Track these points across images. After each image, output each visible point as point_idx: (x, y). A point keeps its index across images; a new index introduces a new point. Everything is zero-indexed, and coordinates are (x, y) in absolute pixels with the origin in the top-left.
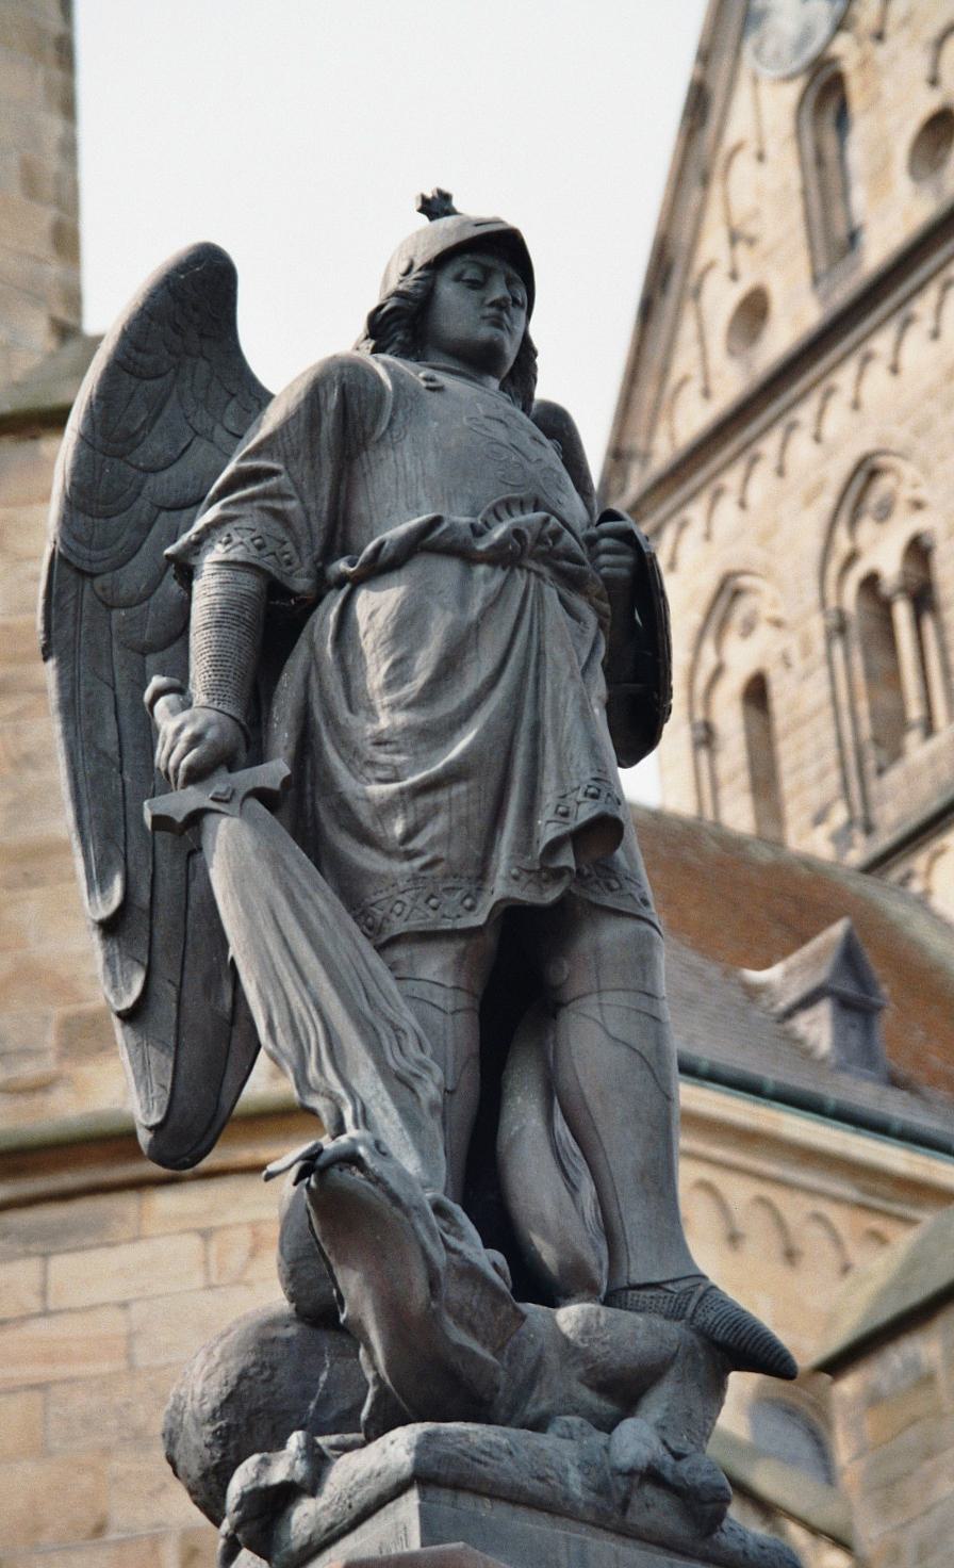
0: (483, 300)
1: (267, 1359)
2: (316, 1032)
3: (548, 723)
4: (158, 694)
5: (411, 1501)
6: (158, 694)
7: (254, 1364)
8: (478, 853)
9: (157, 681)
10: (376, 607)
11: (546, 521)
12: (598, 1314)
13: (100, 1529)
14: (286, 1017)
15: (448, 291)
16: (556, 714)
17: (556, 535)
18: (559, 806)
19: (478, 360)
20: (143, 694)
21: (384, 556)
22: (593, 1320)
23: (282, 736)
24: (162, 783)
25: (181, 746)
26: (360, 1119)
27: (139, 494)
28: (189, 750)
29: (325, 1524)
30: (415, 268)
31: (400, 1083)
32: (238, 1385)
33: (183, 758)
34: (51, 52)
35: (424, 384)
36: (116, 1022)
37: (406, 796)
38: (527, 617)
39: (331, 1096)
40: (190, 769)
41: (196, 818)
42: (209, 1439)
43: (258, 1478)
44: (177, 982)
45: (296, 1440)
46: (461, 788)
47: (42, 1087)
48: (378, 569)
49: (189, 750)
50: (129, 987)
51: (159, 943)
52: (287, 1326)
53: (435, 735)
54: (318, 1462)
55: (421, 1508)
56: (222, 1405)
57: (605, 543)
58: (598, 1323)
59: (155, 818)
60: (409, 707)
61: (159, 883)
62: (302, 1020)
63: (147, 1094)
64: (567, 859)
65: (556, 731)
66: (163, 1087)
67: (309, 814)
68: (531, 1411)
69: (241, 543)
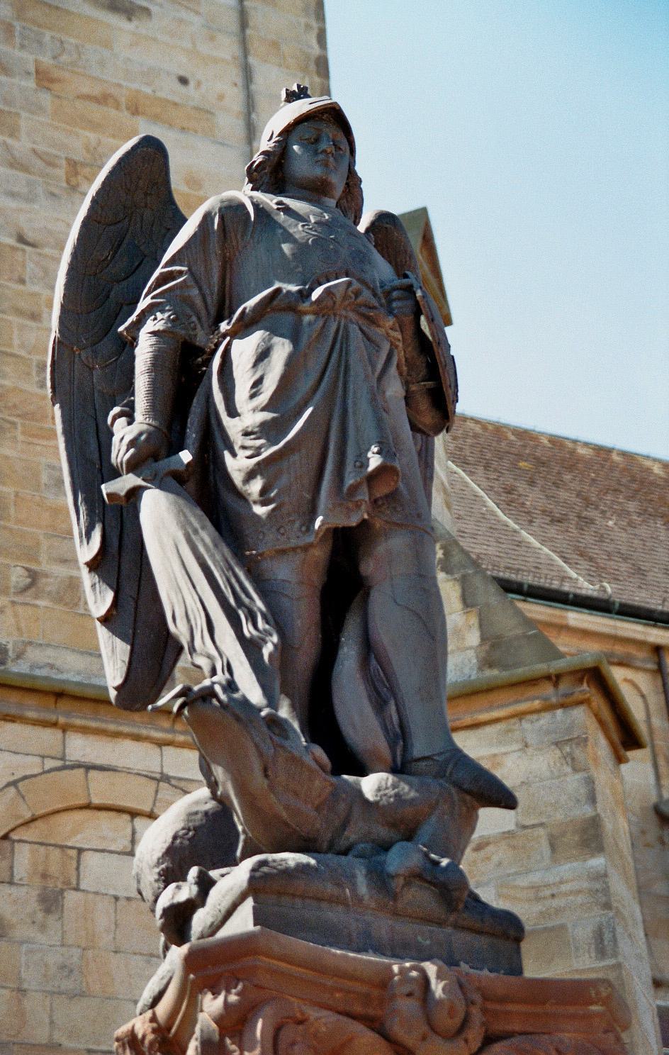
0: (317, 150)
1: (190, 824)
2: (201, 618)
3: (350, 410)
4: (114, 419)
5: (249, 903)
6: (114, 419)
7: (183, 829)
8: (308, 496)
9: (116, 410)
10: (244, 350)
11: (349, 284)
12: (388, 779)
14: (183, 609)
16: (355, 404)
17: (357, 294)
18: (355, 462)
19: (315, 191)
20: (107, 420)
21: (246, 319)
22: (383, 783)
23: (192, 435)
24: (115, 474)
25: (124, 448)
26: (225, 669)
27: (108, 297)
28: (127, 450)
29: (209, 923)
30: (274, 136)
31: (251, 647)
32: (173, 843)
33: (125, 454)
34: (312, 67)
35: (275, 207)
36: (98, 624)
37: (262, 467)
38: (338, 346)
39: (209, 657)
40: (129, 461)
41: (135, 493)
42: (157, 877)
43: (173, 898)
44: (135, 596)
45: (193, 872)
48: (244, 327)
49: (127, 450)
50: (104, 600)
51: (125, 572)
52: (206, 803)
54: (205, 884)
55: (254, 908)
56: (163, 856)
57: (395, 294)
58: (386, 784)
59: (108, 495)
60: (263, 409)
61: (125, 536)
62: (193, 611)
63: (114, 667)
65: (355, 414)
66: (124, 661)
67: (212, 485)
68: (343, 843)
69: (162, 319)
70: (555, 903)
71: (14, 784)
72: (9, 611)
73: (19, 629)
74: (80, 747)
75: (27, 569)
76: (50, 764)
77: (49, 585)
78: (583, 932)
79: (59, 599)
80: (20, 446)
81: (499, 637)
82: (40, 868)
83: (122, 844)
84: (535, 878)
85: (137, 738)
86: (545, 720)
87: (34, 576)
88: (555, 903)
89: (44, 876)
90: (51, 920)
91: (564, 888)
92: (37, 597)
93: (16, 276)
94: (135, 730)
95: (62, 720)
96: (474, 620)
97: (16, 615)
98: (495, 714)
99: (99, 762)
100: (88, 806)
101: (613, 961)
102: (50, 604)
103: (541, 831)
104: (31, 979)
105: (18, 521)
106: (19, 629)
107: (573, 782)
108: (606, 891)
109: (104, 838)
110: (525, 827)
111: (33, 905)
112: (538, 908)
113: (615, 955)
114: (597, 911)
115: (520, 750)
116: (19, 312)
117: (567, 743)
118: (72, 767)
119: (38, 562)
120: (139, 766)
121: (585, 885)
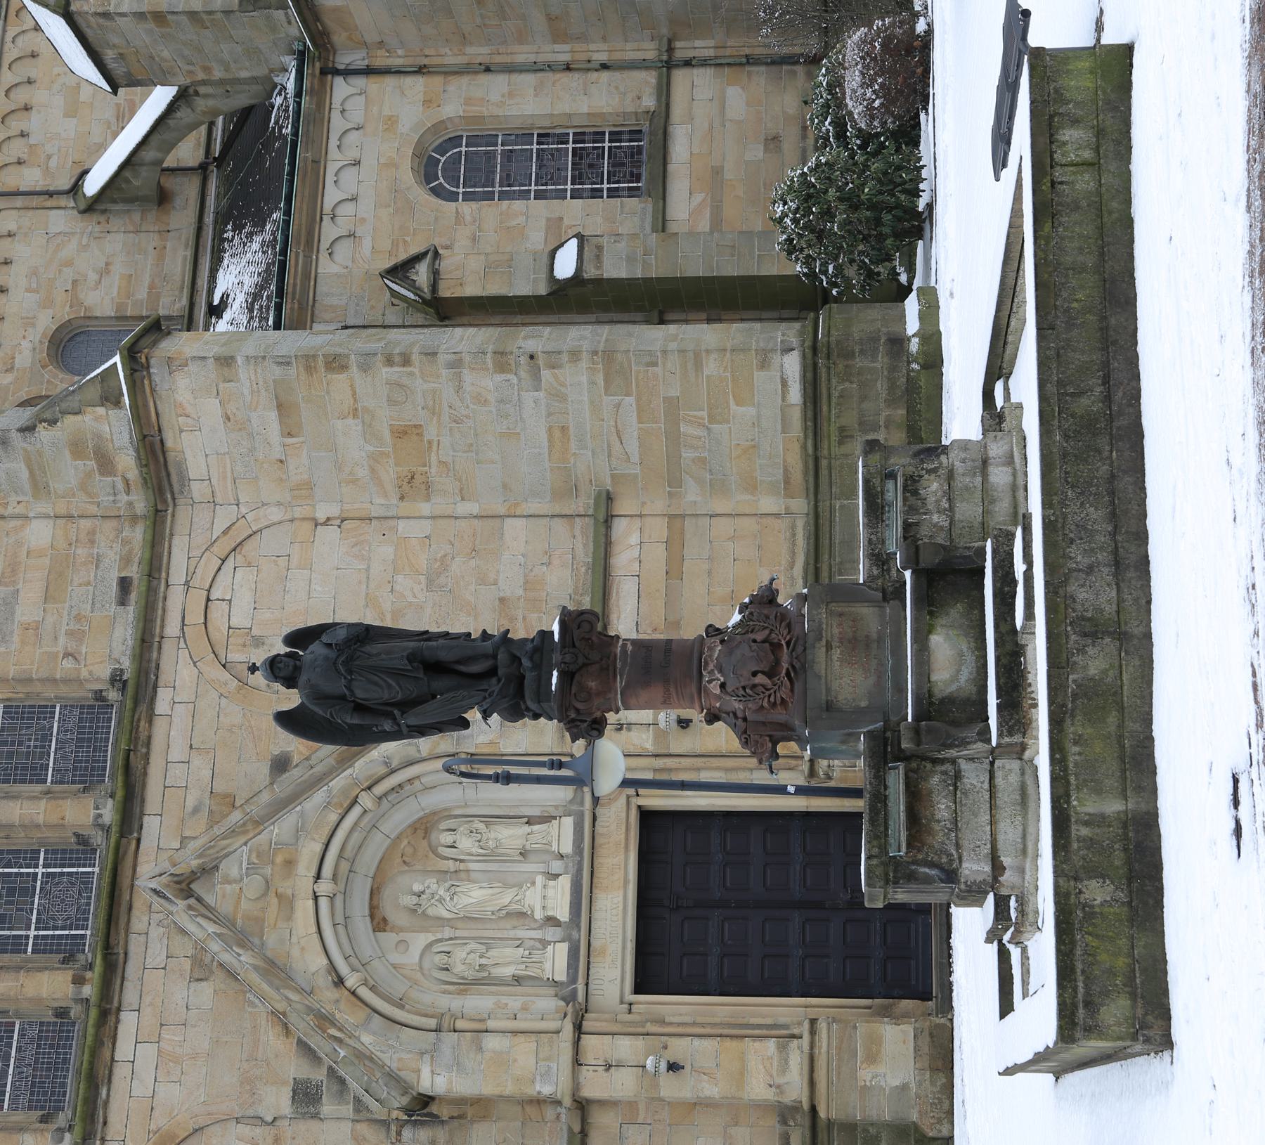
13: (281, 461)
15: (281, 675)
47: (127, 482)
53: (389, 686)
70: (261, 383)
71: (195, 663)
72: (91, 668)
73: (101, 663)
74: (172, 628)
75: (63, 658)
76: (182, 645)
78: (278, 371)
79: (81, 640)
81: (101, 398)
82: (240, 648)
84: (246, 392)
85: (165, 598)
86: (156, 379)
87: (67, 655)
88: (261, 383)
89: (244, 646)
90: (267, 641)
91: (253, 378)
92: (80, 653)
94: (161, 599)
95: (157, 639)
96: (90, 409)
97: (92, 664)
98: (151, 404)
99: (180, 619)
100: (205, 624)
101: (293, 358)
102: (84, 646)
103: (221, 386)
105: (32, 664)
106: (101, 663)
107: (193, 367)
108: (256, 357)
109: (222, 615)
110: (218, 394)
112: (263, 392)
113: (291, 357)
114: (266, 363)
118: (184, 633)
119: (58, 652)
120: (181, 598)
121: (252, 367)
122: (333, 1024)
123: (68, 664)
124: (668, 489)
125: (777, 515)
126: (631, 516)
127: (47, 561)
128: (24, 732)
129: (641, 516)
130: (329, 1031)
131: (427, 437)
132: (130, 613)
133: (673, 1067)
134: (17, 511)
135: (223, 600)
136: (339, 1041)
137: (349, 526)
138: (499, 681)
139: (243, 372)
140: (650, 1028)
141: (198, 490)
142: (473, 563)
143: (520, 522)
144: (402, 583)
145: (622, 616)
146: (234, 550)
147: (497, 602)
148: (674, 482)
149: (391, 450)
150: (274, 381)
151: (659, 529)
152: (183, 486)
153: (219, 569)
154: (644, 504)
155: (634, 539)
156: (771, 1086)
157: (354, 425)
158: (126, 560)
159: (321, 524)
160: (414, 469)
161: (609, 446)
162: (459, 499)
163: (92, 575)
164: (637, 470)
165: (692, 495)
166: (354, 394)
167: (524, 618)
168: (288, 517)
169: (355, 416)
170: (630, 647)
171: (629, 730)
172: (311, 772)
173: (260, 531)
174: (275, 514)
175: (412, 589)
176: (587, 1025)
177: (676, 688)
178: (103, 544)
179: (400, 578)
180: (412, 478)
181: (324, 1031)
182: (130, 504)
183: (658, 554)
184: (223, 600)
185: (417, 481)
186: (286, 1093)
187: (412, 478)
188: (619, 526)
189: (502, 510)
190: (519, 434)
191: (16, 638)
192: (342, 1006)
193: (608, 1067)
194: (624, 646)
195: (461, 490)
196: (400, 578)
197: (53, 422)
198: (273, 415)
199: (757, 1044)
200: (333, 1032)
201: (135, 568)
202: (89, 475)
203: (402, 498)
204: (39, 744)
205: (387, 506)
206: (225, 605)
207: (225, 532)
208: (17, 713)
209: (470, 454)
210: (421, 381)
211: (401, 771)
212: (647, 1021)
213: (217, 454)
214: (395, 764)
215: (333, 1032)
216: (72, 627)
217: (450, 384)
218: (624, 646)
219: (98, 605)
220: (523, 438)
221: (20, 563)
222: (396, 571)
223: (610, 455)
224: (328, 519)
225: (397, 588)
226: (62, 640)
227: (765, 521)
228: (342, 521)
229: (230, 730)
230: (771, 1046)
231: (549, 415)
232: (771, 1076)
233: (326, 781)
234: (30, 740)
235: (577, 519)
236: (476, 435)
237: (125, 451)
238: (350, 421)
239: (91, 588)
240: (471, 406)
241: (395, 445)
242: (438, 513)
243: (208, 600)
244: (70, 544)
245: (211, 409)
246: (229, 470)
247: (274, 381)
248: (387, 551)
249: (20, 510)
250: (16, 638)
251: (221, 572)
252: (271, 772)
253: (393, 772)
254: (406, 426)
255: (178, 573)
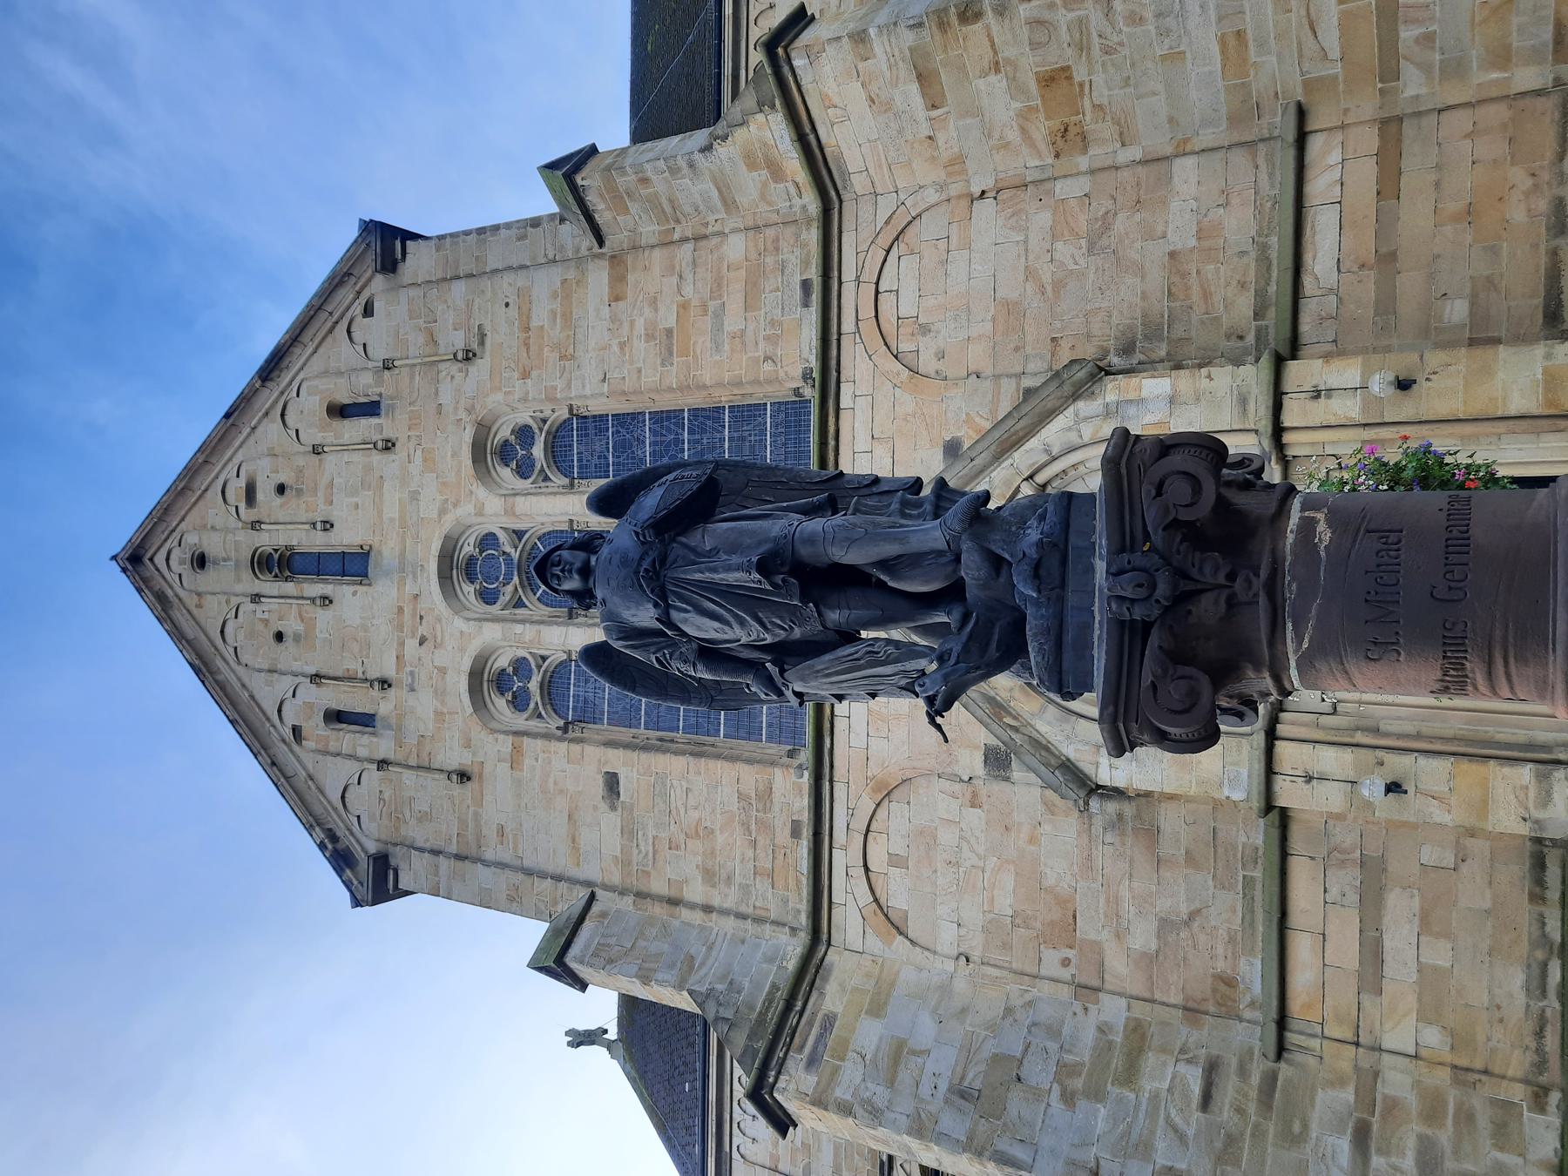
13: (930, 138)
46: (760, 614)
64: (778, 579)
70: (897, 54)
71: (870, 357)
72: (786, 369)
74: (848, 325)
76: (858, 340)
77: (769, 350)
80: (704, 372)
82: (910, 337)
83: (893, 296)
84: (885, 67)
87: (766, 359)
88: (897, 54)
89: (913, 335)
90: (933, 328)
91: (888, 50)
93: (621, 382)
100: (876, 317)
103: (860, 66)
104: (963, 335)
105: (741, 369)
111: (927, 339)
115: (618, 279)
116: (639, 378)
117: (811, 55)
122: (1010, 714)
123: (768, 366)
124: (1380, 85)
125: (1539, 93)
126: (1330, 129)
127: (743, 272)
128: (745, 428)
129: (1343, 127)
130: (1005, 720)
131: (1077, 78)
132: (813, 314)
133: (1393, 788)
134: (715, 229)
135: (891, 291)
136: (1016, 729)
137: (1005, 196)
138: (965, 618)
139: (879, 46)
140: (1360, 738)
141: (859, 183)
142: (1138, 217)
143: (1190, 161)
144: (1063, 250)
145: (1319, 255)
146: (897, 239)
147: (1167, 258)
148: (1389, 72)
149: (1039, 102)
150: (910, 49)
151: (1369, 139)
152: (844, 181)
153: (885, 260)
154: (1346, 111)
155: (1335, 157)
156: (1525, 820)
157: (997, 82)
158: (806, 264)
159: (977, 199)
160: (1066, 120)
161: (1300, 44)
162: (1119, 145)
163: (780, 280)
164: (1338, 69)
165: (1413, 85)
166: (993, 45)
167: (1198, 272)
168: (944, 197)
169: (997, 71)
170: (1324, 533)
171: (1329, 397)
172: (971, 465)
173: (920, 215)
174: (932, 196)
175: (1073, 256)
176: (1281, 729)
177: (1490, 665)
178: (785, 250)
179: (1059, 245)
180: (1066, 130)
181: (1001, 720)
182: (804, 207)
183: (1366, 173)
184: (891, 291)
185: (1073, 130)
186: (979, 757)
187: (1066, 130)
188: (1315, 144)
189: (1169, 150)
190: (1184, 53)
191: (727, 347)
192: (1017, 694)
193: (1309, 778)
194: (1307, 526)
195: (1121, 134)
196: (1059, 245)
197: (725, 138)
198: (914, 88)
199: (1507, 770)
200: (1008, 720)
201: (814, 270)
202: (765, 185)
203: (1057, 156)
204: (757, 438)
205: (1042, 168)
206: (893, 296)
207: (887, 222)
208: (738, 411)
209: (1127, 90)
210: (1064, 12)
211: (1063, 458)
212: (1357, 729)
213: (869, 141)
214: (1055, 452)
215: (1008, 720)
216: (768, 332)
217: (1098, 6)
218: (1307, 526)
219: (787, 309)
220: (1188, 55)
221: (723, 277)
222: (1054, 237)
223: (1301, 56)
224: (983, 192)
225: (1057, 256)
226: (762, 345)
227: (1521, 103)
228: (998, 192)
229: (905, 419)
230: (1526, 773)
231: (1220, 19)
232: (1527, 808)
233: (986, 473)
234: (750, 435)
235: (1261, 146)
236: (1133, 65)
237: (789, 154)
238: (993, 78)
239: (780, 293)
240: (1125, 29)
241: (1043, 97)
242: (1097, 165)
243: (877, 292)
244: (760, 254)
245: (854, 94)
246: (883, 157)
247: (910, 49)
248: (1043, 219)
249: (717, 228)
250: (727, 347)
251: (887, 263)
252: (944, 457)
253: (1055, 459)
254: (1052, 71)
255: (849, 274)
